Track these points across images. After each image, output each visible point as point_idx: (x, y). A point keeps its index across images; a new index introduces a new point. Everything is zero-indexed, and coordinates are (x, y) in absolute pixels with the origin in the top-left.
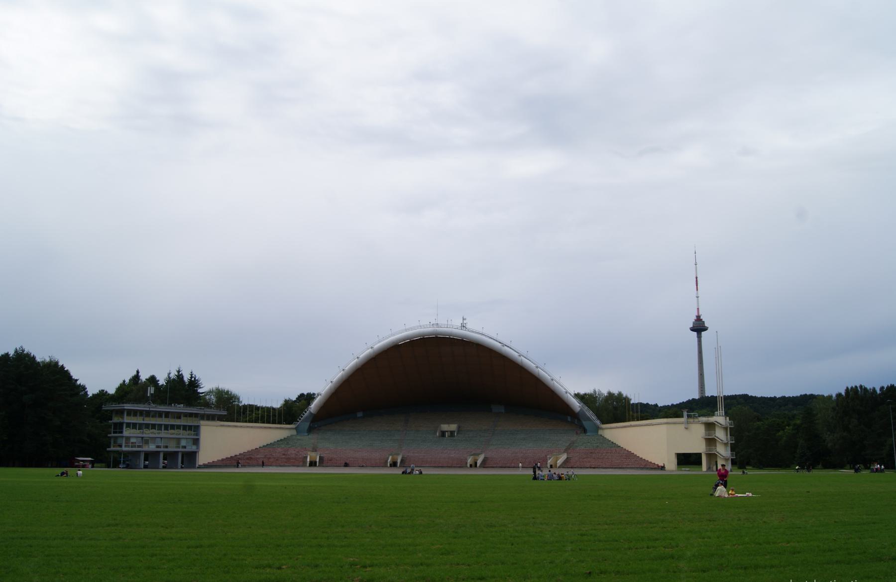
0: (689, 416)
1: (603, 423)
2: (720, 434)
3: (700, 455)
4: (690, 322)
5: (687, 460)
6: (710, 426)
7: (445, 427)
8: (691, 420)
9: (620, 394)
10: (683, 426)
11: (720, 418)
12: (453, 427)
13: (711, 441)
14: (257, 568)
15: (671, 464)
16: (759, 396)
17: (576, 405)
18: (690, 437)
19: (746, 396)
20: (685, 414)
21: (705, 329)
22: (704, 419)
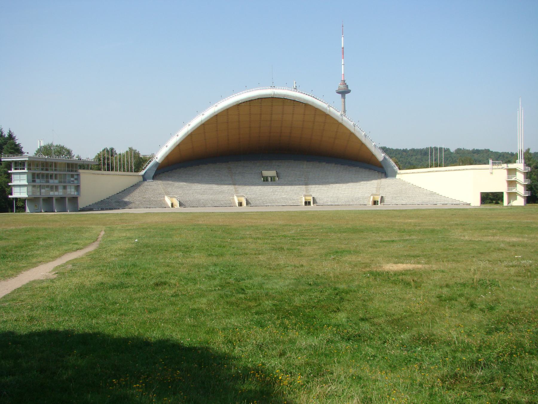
0: (493, 164)
1: (400, 169)
2: (520, 177)
3: (502, 193)
4: (338, 85)
5: (491, 198)
6: (512, 172)
7: (266, 173)
8: (495, 167)
9: (474, 149)
10: (489, 171)
11: (520, 165)
12: (272, 173)
13: (512, 183)
14: (393, 241)
15: (476, 202)
16: (394, 148)
17: (380, 156)
18: (492, 178)
19: (488, 150)
20: (491, 161)
21: (349, 92)
22: (505, 166)
